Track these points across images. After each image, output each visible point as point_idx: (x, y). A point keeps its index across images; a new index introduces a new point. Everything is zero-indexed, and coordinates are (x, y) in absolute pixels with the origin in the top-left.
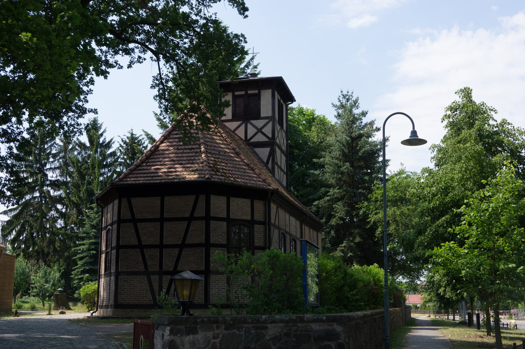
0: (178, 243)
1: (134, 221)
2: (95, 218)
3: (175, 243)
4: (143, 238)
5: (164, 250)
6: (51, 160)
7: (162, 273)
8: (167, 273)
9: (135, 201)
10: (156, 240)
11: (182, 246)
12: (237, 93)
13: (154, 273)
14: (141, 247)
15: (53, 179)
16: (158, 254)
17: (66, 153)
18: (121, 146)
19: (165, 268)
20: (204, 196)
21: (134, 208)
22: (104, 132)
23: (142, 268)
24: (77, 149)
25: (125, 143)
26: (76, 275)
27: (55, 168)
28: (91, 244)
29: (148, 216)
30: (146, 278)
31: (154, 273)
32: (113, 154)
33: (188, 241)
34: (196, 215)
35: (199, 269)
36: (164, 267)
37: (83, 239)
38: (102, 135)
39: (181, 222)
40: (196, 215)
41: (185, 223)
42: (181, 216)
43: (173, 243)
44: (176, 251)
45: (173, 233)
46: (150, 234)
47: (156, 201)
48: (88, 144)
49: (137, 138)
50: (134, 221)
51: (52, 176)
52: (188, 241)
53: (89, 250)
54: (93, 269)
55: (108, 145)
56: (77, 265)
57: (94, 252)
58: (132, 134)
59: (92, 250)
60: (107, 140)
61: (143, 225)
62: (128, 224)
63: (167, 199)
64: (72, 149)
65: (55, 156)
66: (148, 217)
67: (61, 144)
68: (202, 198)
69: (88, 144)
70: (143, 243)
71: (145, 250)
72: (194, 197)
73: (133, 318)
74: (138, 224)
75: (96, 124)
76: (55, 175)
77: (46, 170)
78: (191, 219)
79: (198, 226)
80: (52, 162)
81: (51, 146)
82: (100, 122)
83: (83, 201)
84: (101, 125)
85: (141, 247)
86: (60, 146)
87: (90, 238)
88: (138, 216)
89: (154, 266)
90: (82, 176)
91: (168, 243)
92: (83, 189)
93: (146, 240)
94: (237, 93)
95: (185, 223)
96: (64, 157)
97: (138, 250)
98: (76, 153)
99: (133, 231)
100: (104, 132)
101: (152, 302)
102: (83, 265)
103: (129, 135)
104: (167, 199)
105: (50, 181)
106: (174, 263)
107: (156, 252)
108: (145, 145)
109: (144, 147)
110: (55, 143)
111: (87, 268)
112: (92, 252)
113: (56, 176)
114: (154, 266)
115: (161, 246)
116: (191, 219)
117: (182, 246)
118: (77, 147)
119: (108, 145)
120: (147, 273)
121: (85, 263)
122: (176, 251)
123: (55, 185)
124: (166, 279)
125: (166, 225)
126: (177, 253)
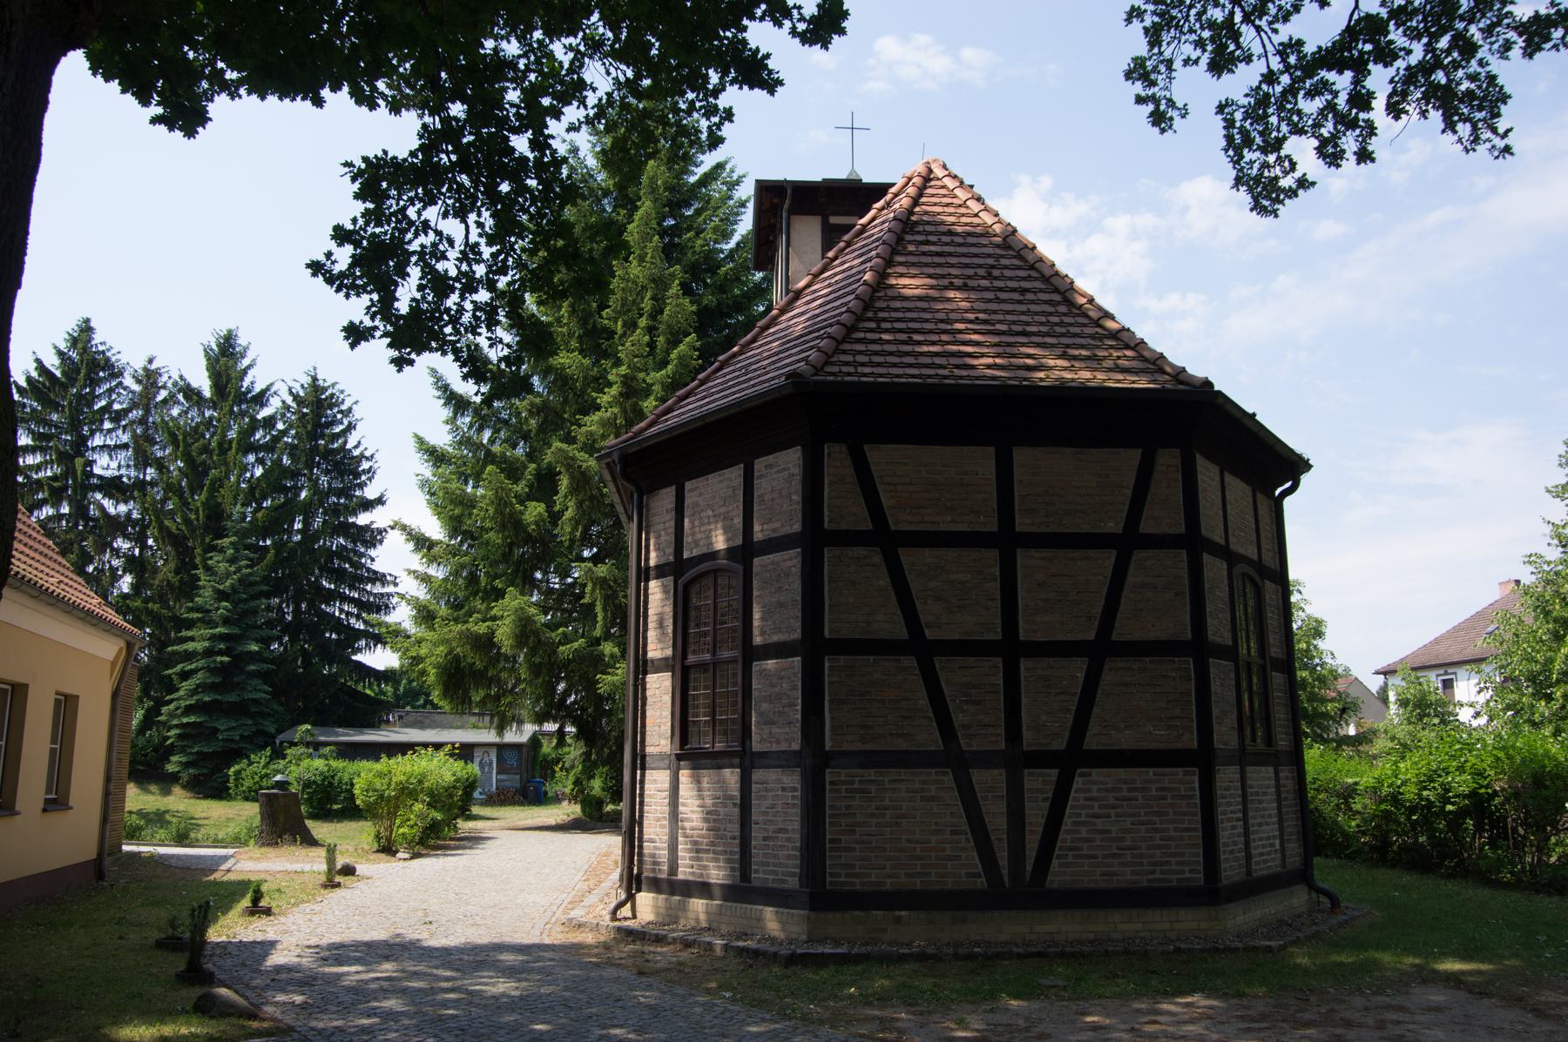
0: (1081, 637)
1: (886, 539)
2: (228, 575)
3: (1070, 637)
4: (928, 611)
5: (1024, 664)
6: (107, 425)
7: (1017, 759)
8: (1040, 759)
9: (880, 457)
10: (984, 622)
11: (1101, 649)
12: (834, 220)
13: (986, 760)
14: (921, 648)
15: (108, 474)
16: (999, 680)
17: (147, 412)
18: (288, 408)
19: (1029, 739)
20: (1176, 452)
21: (880, 488)
22: (249, 367)
23: (928, 737)
24: (179, 403)
25: (296, 397)
26: (172, 715)
27: (117, 447)
28: (213, 638)
29: (946, 524)
30: (949, 779)
31: (986, 760)
32: (269, 422)
33: (1124, 630)
34: (1146, 527)
35: (1179, 746)
36: (1027, 735)
37: (190, 624)
38: (245, 372)
39: (1090, 552)
40: (1146, 527)
41: (1108, 558)
42: (1085, 528)
43: (1060, 637)
44: (1077, 669)
45: (1059, 593)
46: (957, 593)
47: (980, 462)
48: (207, 393)
49: (325, 389)
50: (886, 539)
51: (104, 466)
52: (1124, 630)
53: (208, 653)
54: (219, 702)
55: (261, 399)
56: (177, 690)
57: (226, 659)
58: (315, 379)
59: (220, 653)
60: (258, 389)
61: (928, 556)
62: (859, 551)
63: (1022, 457)
64: (165, 401)
65: (117, 417)
66: (943, 527)
67: (137, 388)
68: (1168, 461)
69: (207, 393)
70: (929, 634)
71: (938, 662)
72: (1136, 455)
73: (956, 956)
74: (901, 551)
75: (232, 346)
76: (114, 465)
77: (94, 449)
78: (1128, 542)
79: (1155, 572)
80: (110, 431)
81: (111, 391)
82: (242, 341)
83: (193, 531)
84: (181, 377)
85: (921, 648)
86: (133, 392)
87: (210, 624)
88: (901, 521)
89: (981, 728)
90: (196, 472)
91: (1040, 637)
92: (200, 498)
93: (940, 623)
94: (834, 220)
95: (1108, 558)
96: (142, 421)
97: (910, 662)
98: (175, 412)
99: (884, 581)
100: (249, 367)
101: (981, 883)
102: (194, 692)
103: (306, 380)
104: (1022, 457)
105: (100, 477)
106: (1071, 717)
107: (990, 671)
108: (344, 407)
109: (341, 412)
110: (121, 383)
111: (207, 699)
112: (219, 659)
113: (119, 467)
114: (981, 728)
115: (1011, 649)
116: (1128, 542)
117: (1101, 649)
118: (180, 397)
119: (261, 399)
120: (955, 760)
121: (198, 686)
122: (1077, 669)
123: (113, 487)
124: (1039, 784)
125: (1026, 560)
126: (1081, 675)
